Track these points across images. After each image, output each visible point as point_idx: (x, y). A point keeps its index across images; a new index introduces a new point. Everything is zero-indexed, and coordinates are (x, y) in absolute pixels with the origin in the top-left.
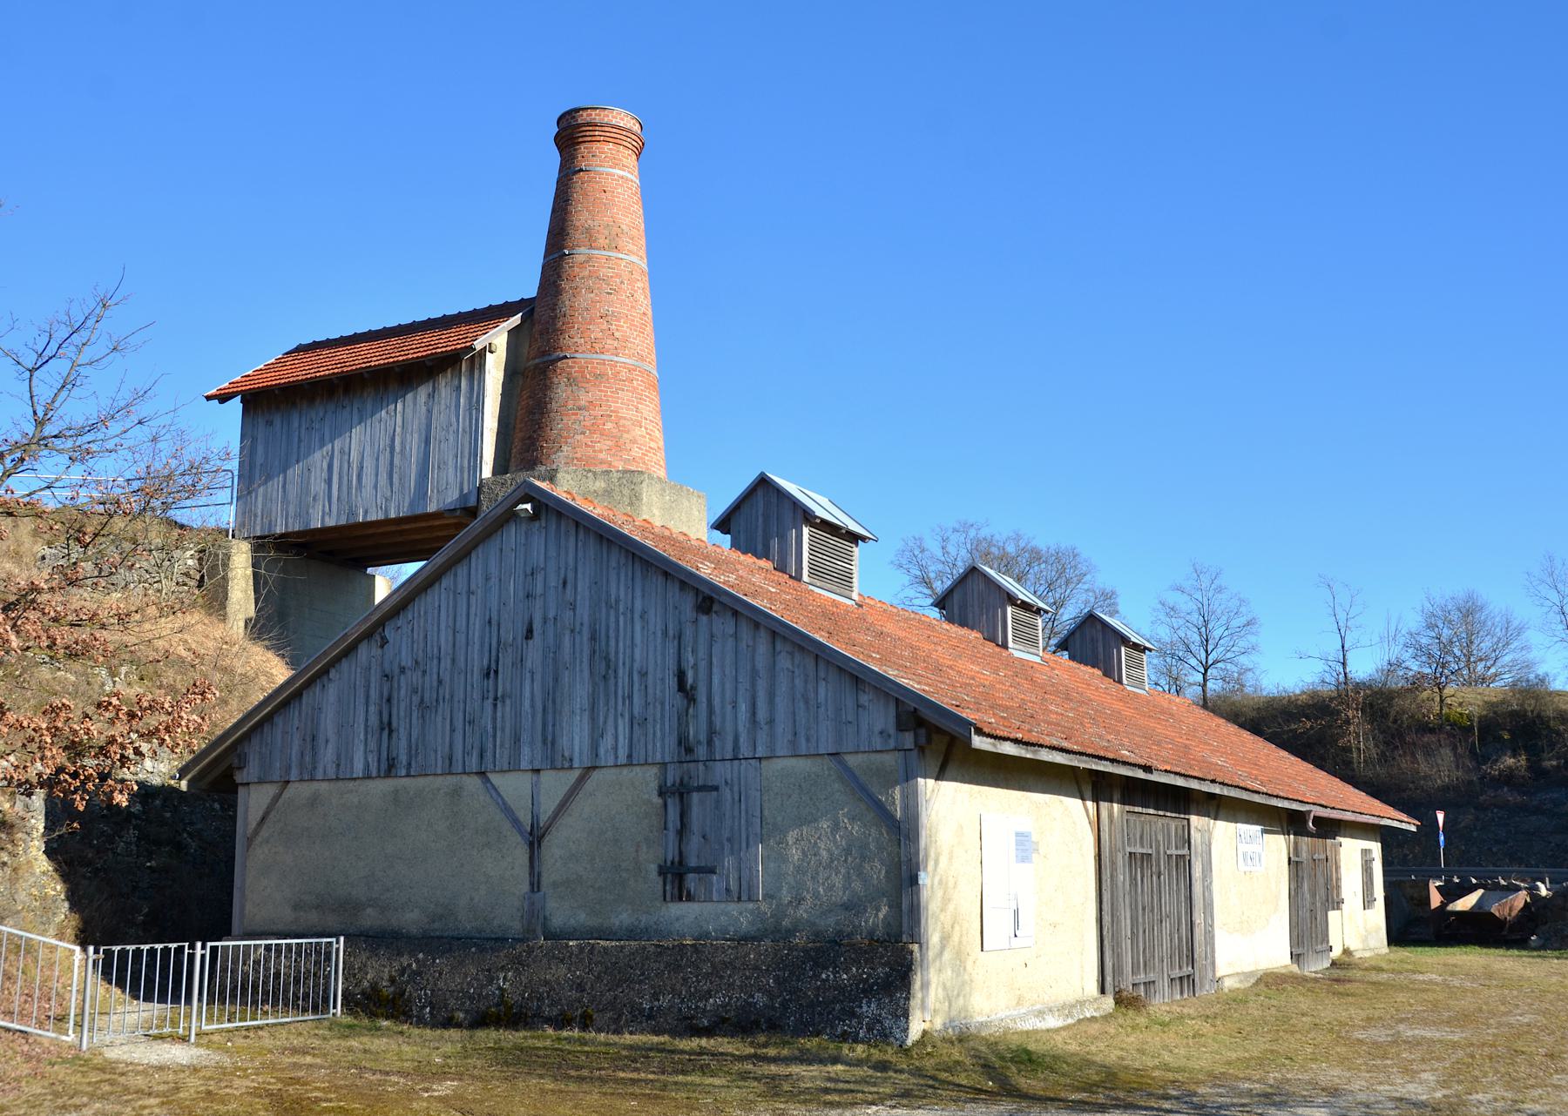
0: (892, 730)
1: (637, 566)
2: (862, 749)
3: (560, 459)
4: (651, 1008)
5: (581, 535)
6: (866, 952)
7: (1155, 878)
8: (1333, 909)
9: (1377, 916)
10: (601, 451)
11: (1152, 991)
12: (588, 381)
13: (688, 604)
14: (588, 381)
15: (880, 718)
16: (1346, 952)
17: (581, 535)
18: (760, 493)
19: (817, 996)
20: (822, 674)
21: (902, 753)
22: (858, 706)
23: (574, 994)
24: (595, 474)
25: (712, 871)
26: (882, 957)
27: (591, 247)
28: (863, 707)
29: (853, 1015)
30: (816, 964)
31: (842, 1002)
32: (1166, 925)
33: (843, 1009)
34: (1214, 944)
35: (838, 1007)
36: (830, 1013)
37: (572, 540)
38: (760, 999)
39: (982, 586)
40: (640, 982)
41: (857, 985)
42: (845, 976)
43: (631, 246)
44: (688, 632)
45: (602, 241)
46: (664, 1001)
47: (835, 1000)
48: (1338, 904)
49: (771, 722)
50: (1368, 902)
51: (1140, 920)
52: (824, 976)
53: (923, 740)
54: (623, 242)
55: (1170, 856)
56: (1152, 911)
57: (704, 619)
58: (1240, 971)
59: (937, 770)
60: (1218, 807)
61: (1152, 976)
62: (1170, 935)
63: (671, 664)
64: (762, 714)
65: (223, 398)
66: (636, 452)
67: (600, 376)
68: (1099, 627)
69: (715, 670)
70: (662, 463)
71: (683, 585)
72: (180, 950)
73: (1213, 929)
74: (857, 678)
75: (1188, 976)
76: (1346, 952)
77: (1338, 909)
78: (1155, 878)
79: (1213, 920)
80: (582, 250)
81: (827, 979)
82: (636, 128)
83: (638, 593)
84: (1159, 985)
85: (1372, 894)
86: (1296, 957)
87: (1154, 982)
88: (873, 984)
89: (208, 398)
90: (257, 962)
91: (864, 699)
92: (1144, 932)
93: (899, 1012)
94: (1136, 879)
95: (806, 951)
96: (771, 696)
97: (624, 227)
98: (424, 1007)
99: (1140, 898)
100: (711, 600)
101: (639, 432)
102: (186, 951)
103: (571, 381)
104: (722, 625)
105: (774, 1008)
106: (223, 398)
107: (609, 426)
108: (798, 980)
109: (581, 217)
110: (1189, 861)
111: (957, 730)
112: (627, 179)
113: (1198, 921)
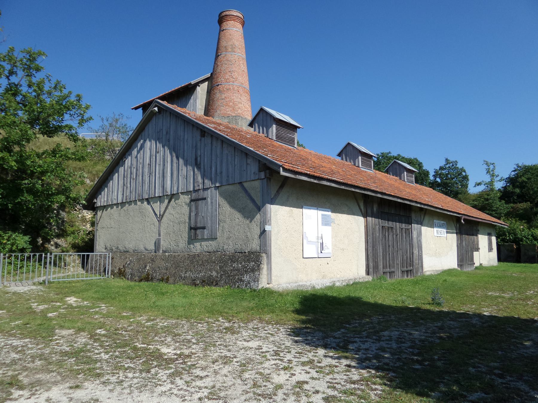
0: (257, 172)
1: (186, 124)
2: (248, 180)
3: (216, 114)
4: (184, 277)
5: (172, 116)
6: (247, 256)
7: (394, 236)
8: (476, 251)
9: (494, 254)
10: (228, 111)
11: (393, 275)
12: (225, 91)
13: (198, 134)
14: (225, 91)
15: (253, 168)
16: (481, 264)
17: (172, 116)
18: (261, 114)
19: (231, 273)
20: (236, 154)
21: (261, 180)
22: (247, 164)
23: (165, 271)
24: (225, 117)
25: (204, 228)
26: (252, 259)
27: (226, 52)
28: (249, 164)
29: (241, 280)
30: (232, 261)
31: (238, 275)
32: (400, 252)
33: (238, 278)
34: (422, 260)
35: (237, 277)
36: (234, 279)
37: (169, 118)
38: (214, 274)
39: (351, 148)
40: (182, 267)
41: (244, 269)
42: (240, 266)
43: (239, 51)
44: (199, 144)
45: (230, 50)
46: (187, 275)
47: (236, 275)
48: (477, 249)
49: (221, 173)
50: (490, 249)
51: (387, 250)
52: (234, 266)
53: (268, 175)
54: (237, 50)
55: (402, 229)
56: (393, 247)
57: (203, 139)
58: (434, 269)
59: (278, 187)
60: (425, 214)
61: (393, 270)
62: (402, 256)
63: (194, 157)
64: (218, 171)
65: (136, 108)
66: (240, 111)
67: (228, 89)
68: (397, 164)
69: (206, 156)
70: (249, 115)
71: (198, 128)
72: (41, 255)
73: (422, 255)
74: (246, 153)
75: (411, 271)
76: (481, 264)
77: (478, 251)
78: (394, 236)
79: (422, 252)
80: (224, 53)
81: (235, 267)
82: (242, 17)
83: (186, 133)
84: (396, 273)
85: (492, 247)
86: (460, 265)
87: (394, 272)
88: (249, 269)
89: (132, 109)
90: (96, 261)
91: (249, 161)
92: (389, 254)
93: (256, 280)
94: (385, 235)
95: (229, 256)
96: (221, 162)
97: (236, 45)
98: (129, 275)
99: (387, 242)
100: (205, 132)
101: (240, 105)
102: (43, 256)
103: (220, 92)
104: (208, 140)
105: (217, 277)
106: (136, 108)
107: (231, 104)
108: (226, 267)
109: (223, 43)
110: (411, 231)
111: (275, 168)
112: (238, 31)
113: (415, 252)
